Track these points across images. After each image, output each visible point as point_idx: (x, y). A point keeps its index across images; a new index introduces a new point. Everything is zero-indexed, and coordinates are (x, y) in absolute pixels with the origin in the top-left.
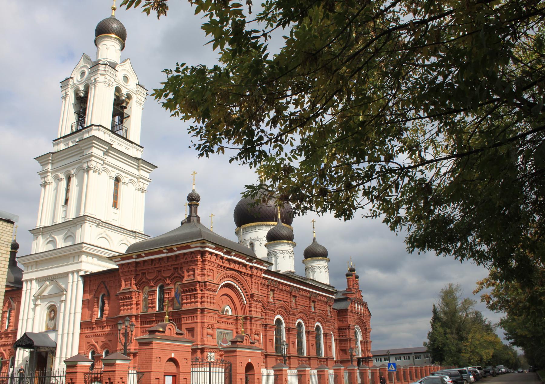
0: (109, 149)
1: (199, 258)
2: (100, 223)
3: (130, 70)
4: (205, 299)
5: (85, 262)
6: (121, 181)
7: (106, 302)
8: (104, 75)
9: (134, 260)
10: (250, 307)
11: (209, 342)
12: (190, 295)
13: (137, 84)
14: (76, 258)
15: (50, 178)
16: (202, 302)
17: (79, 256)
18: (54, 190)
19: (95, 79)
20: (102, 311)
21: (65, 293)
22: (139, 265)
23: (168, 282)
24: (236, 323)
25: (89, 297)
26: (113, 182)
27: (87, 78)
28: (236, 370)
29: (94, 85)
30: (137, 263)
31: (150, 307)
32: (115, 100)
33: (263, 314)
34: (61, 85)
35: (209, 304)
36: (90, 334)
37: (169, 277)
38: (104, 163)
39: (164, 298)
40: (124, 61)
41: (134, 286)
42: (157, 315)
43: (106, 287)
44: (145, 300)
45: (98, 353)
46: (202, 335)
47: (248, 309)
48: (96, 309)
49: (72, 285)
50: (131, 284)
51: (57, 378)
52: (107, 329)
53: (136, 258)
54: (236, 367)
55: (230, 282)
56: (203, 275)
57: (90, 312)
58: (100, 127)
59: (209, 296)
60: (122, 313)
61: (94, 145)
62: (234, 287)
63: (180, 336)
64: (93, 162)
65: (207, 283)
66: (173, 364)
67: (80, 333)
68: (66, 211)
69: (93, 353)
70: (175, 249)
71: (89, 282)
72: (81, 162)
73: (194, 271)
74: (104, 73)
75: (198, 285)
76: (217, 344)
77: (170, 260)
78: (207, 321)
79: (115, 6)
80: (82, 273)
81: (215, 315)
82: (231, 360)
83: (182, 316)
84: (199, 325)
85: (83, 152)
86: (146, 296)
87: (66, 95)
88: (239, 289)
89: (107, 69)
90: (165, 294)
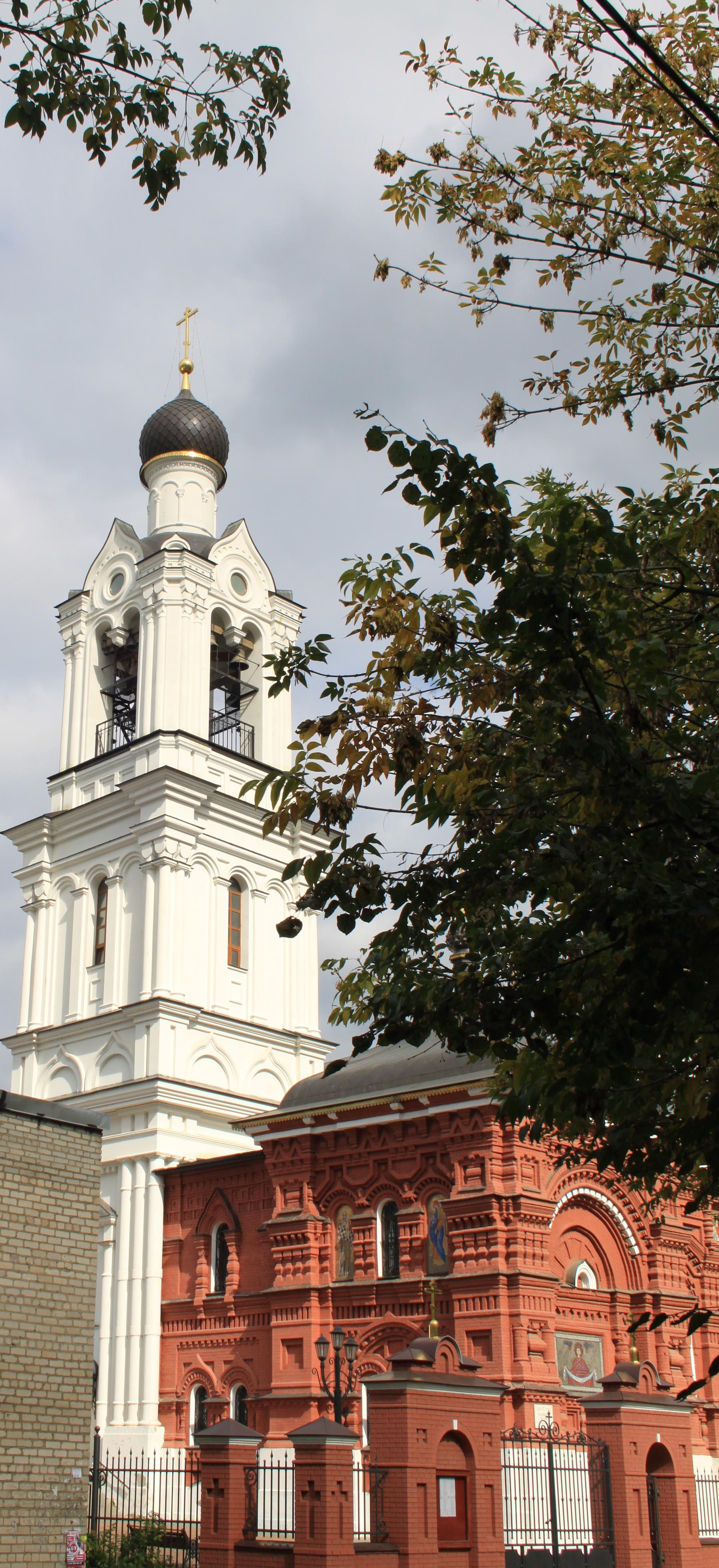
0: (209, 799)
1: (496, 1127)
2: (198, 1016)
3: (247, 555)
4: (519, 1248)
5: (165, 1132)
6: (246, 887)
7: (232, 1249)
8: (178, 581)
9: (306, 1131)
10: (651, 1264)
11: (535, 1372)
12: (475, 1234)
13: (271, 594)
14: (140, 1119)
15: (48, 888)
16: (509, 1256)
17: (147, 1116)
18: (61, 922)
19: (155, 596)
20: (222, 1273)
21: (113, 1220)
22: (322, 1144)
23: (410, 1194)
24: (613, 1313)
25: (180, 1233)
26: (224, 893)
27: (131, 591)
28: (621, 1464)
29: (154, 611)
30: (316, 1139)
31: (359, 1267)
32: (213, 647)
33: (693, 1281)
34: (57, 612)
35: (529, 1260)
36: (190, 1340)
37: (410, 1182)
38: (199, 841)
39: (397, 1242)
40: (231, 529)
41: (312, 1206)
42: (380, 1289)
43: (229, 1207)
44: (343, 1245)
45: (215, 1395)
46: (515, 1353)
47: (645, 1270)
48: (204, 1267)
49: (133, 1199)
50: (301, 1199)
51: (116, 1473)
52: (239, 1327)
53: (312, 1126)
54: (621, 1456)
55: (587, 1192)
56: (507, 1176)
57: (187, 1277)
58: (180, 738)
59: (530, 1236)
60: (281, 1283)
61: (168, 792)
62: (601, 1204)
63: (470, 1374)
64: (167, 843)
65: (522, 1200)
66: (457, 1448)
67: (162, 1337)
68: (100, 983)
69: (201, 1394)
70: (424, 1101)
71: (178, 1188)
72: (134, 842)
73: (482, 1166)
74: (178, 575)
75: (495, 1205)
76: (557, 1378)
77: (412, 1130)
78: (527, 1311)
79: (188, 362)
80: (158, 1164)
81: (550, 1294)
82: (606, 1435)
83: (455, 1296)
84: (504, 1322)
85: (138, 812)
86: (347, 1233)
87: (75, 643)
88: (615, 1210)
89: (186, 564)
90: (402, 1230)
